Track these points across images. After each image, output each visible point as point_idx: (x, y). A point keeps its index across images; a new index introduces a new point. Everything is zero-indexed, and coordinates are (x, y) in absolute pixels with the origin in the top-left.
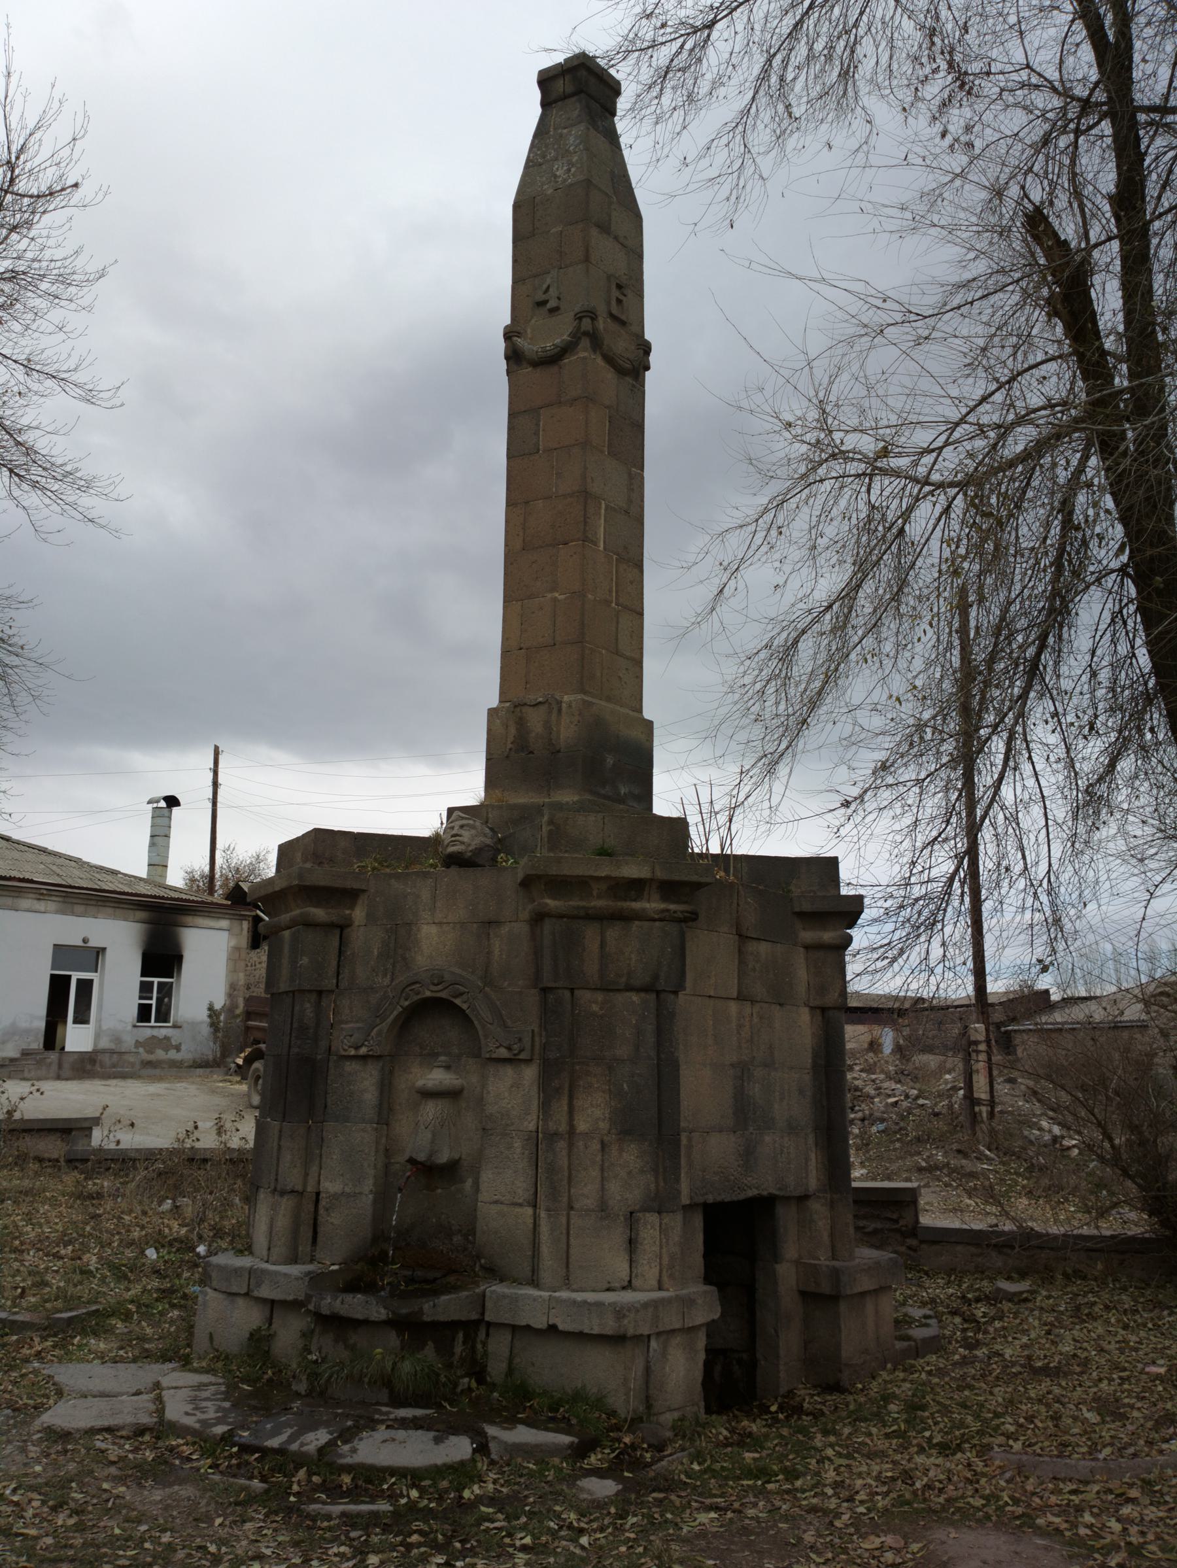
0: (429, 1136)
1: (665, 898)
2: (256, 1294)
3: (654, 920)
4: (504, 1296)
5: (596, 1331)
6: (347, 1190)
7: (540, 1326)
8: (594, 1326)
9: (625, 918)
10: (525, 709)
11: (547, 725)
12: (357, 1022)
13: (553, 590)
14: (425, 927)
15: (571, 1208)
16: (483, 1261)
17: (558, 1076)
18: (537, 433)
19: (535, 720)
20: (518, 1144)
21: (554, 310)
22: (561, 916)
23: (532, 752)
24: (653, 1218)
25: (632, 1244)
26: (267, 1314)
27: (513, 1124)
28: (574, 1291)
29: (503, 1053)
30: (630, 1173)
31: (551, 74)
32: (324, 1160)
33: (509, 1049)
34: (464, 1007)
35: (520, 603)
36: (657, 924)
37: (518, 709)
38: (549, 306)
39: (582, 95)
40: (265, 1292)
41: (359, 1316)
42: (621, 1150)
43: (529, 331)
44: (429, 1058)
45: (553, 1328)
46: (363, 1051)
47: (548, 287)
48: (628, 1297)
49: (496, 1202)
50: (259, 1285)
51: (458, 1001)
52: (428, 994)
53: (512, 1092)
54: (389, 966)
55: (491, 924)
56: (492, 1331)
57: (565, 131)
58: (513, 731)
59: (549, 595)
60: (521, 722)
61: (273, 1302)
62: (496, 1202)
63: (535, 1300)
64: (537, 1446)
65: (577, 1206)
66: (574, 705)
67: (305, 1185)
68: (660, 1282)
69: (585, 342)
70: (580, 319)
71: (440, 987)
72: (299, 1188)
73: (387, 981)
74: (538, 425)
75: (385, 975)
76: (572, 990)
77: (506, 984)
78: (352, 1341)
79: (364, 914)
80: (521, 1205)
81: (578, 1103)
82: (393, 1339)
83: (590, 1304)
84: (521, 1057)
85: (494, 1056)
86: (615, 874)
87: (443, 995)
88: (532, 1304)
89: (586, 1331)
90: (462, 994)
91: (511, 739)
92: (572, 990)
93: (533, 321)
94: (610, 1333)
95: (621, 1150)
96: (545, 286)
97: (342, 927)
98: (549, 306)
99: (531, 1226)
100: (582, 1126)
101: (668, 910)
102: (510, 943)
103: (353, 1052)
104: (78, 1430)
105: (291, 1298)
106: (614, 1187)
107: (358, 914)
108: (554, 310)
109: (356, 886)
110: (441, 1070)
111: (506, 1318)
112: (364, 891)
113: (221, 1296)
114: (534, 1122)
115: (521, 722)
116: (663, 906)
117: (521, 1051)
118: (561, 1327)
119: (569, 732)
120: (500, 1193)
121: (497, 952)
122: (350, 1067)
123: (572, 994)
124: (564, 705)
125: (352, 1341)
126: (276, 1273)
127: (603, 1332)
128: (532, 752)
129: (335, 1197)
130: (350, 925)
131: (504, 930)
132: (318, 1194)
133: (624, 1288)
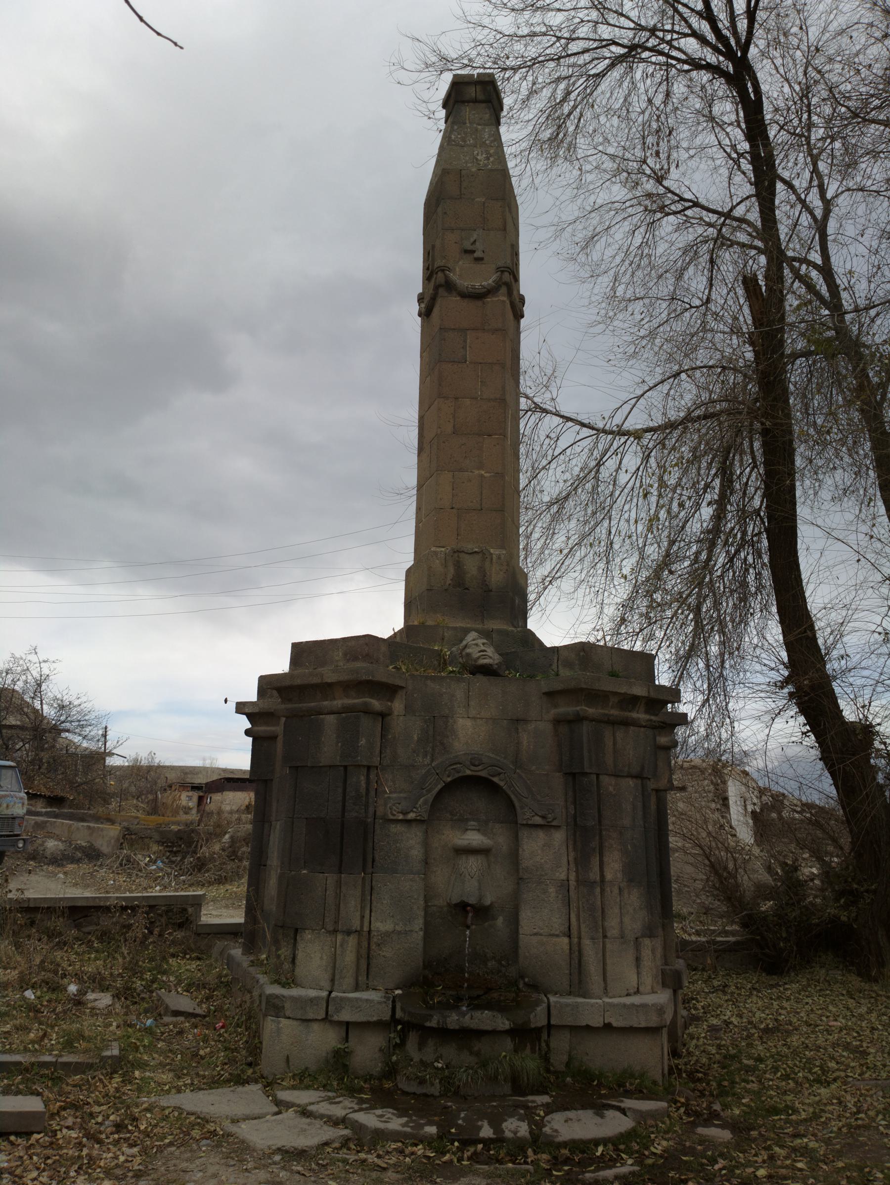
0: (476, 884)
1: (647, 712)
2: (335, 1018)
3: (641, 726)
4: (567, 1005)
5: (643, 1025)
6: (398, 928)
7: (598, 1025)
8: (641, 1022)
9: (626, 723)
10: (461, 555)
11: (481, 569)
12: (400, 792)
13: (480, 468)
14: (461, 720)
15: (605, 937)
16: (526, 980)
17: (586, 839)
18: (464, 348)
19: (471, 566)
20: (552, 890)
21: (479, 260)
22: (592, 720)
23: (467, 589)
24: (647, 941)
25: (638, 960)
26: (344, 1035)
27: (546, 874)
28: (611, 998)
29: (538, 820)
30: (634, 909)
31: (466, 80)
32: (374, 904)
33: (543, 817)
34: (502, 784)
35: (451, 473)
36: (642, 729)
37: (456, 555)
38: (476, 255)
39: (490, 104)
40: (346, 1016)
41: (489, 1028)
42: (629, 893)
43: (457, 269)
44: (461, 823)
45: (608, 1027)
46: (411, 816)
47: (475, 241)
48: (636, 1000)
49: (535, 934)
50: (338, 1010)
51: (496, 780)
52: (468, 772)
53: (546, 851)
54: (429, 749)
55: (517, 722)
56: (552, 1032)
57: (479, 127)
58: (451, 570)
59: (477, 472)
60: (458, 565)
61: (348, 1024)
62: (535, 934)
63: (592, 1006)
64: (657, 1110)
65: (609, 934)
66: (502, 557)
67: (362, 926)
68: (652, 988)
69: (504, 290)
70: (502, 272)
71: (480, 768)
72: (359, 929)
73: (427, 760)
74: (465, 341)
75: (425, 756)
76: (598, 775)
77: (534, 768)
78: (476, 1049)
79: (402, 706)
80: (557, 936)
81: (606, 859)
82: (509, 1044)
83: (637, 1006)
84: (553, 824)
85: (530, 822)
86: (629, 692)
87: (483, 774)
88: (591, 1009)
89: (635, 1026)
90: (499, 774)
91: (450, 576)
92: (598, 775)
93: (460, 263)
94: (654, 1026)
95: (629, 893)
96: (472, 240)
97: (383, 716)
98: (476, 255)
99: (568, 951)
100: (609, 876)
101: (651, 720)
102: (538, 736)
103: (401, 817)
104: (312, 1148)
105: (375, 1019)
106: (627, 920)
107: (398, 706)
108: (479, 260)
109: (398, 682)
110: (475, 832)
111: (569, 1021)
112: (402, 688)
113: (295, 1023)
114: (564, 873)
115: (458, 565)
116: (647, 717)
117: (554, 819)
118: (615, 1024)
119: (468, 577)
120: (541, 928)
121: (525, 743)
122: (394, 829)
123: (598, 778)
124: (494, 556)
125: (476, 1049)
126: (357, 999)
127: (650, 1025)
128: (467, 589)
129: (387, 934)
130: (389, 715)
131: (531, 727)
132: (369, 932)
133: (635, 993)
